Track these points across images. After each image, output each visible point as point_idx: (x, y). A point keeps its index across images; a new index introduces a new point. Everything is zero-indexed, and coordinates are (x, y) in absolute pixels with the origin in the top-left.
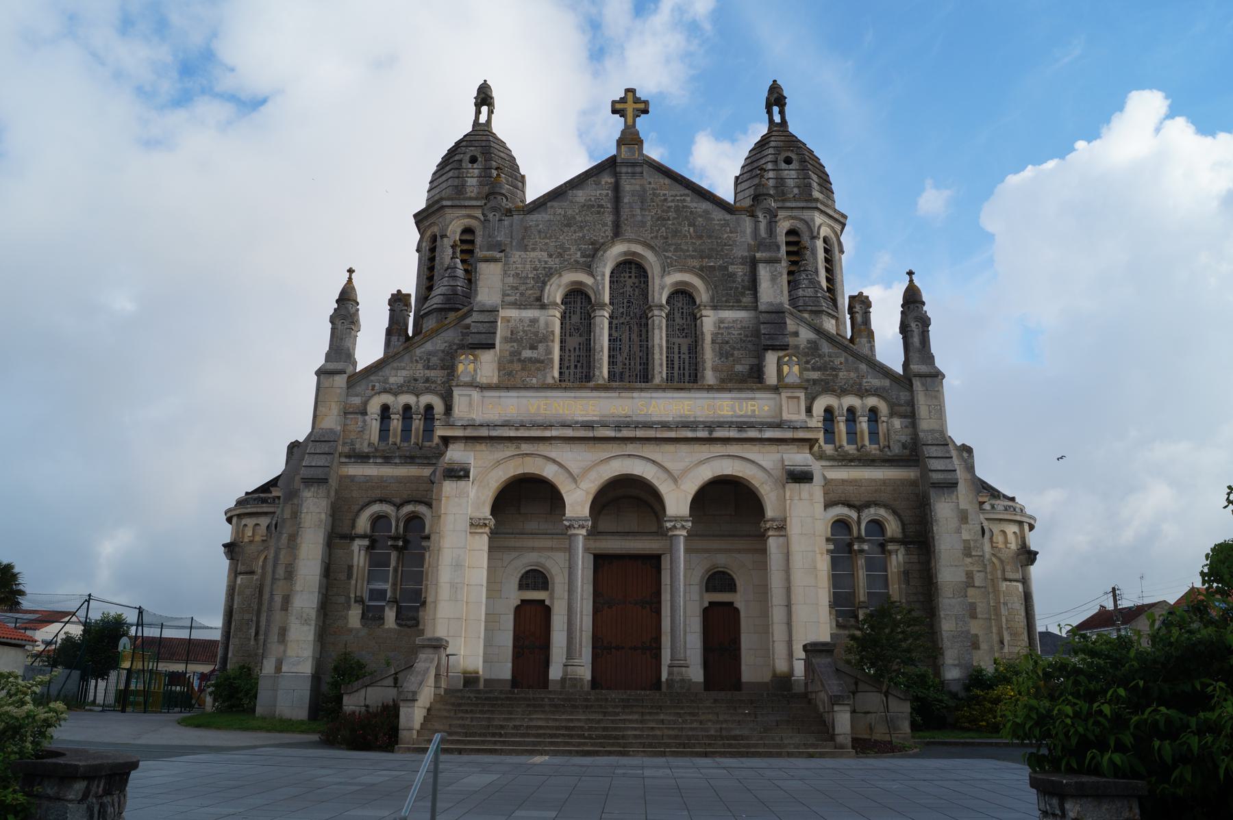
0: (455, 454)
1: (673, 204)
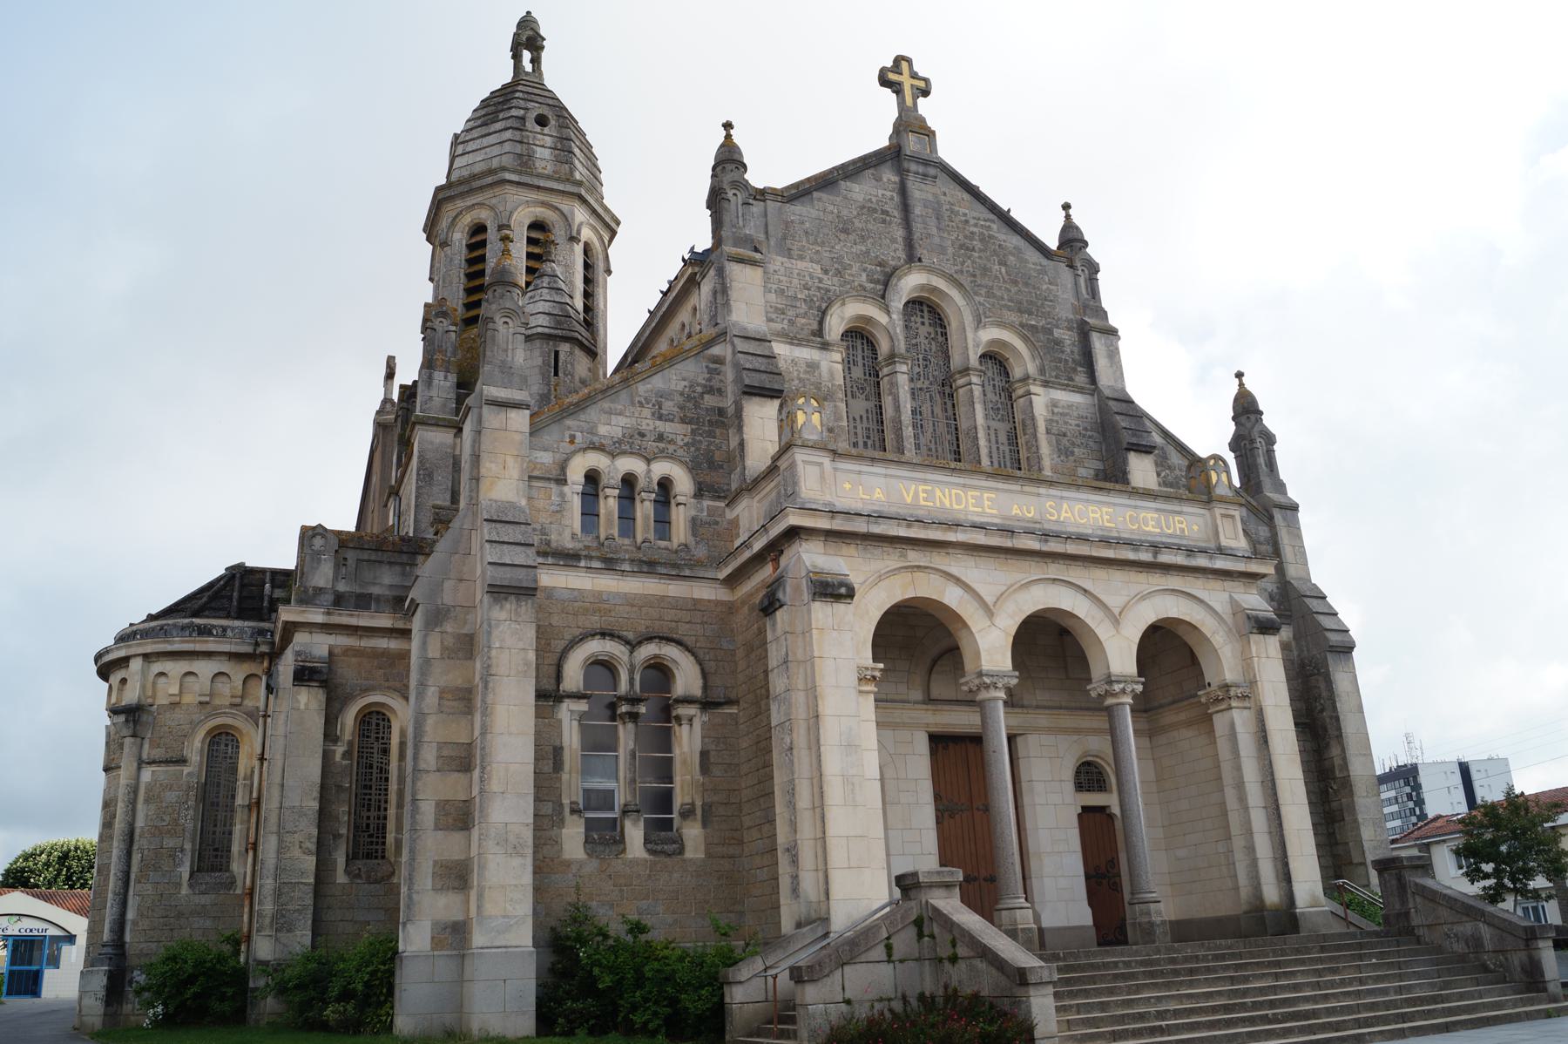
0: (811, 557)
1: (975, 230)
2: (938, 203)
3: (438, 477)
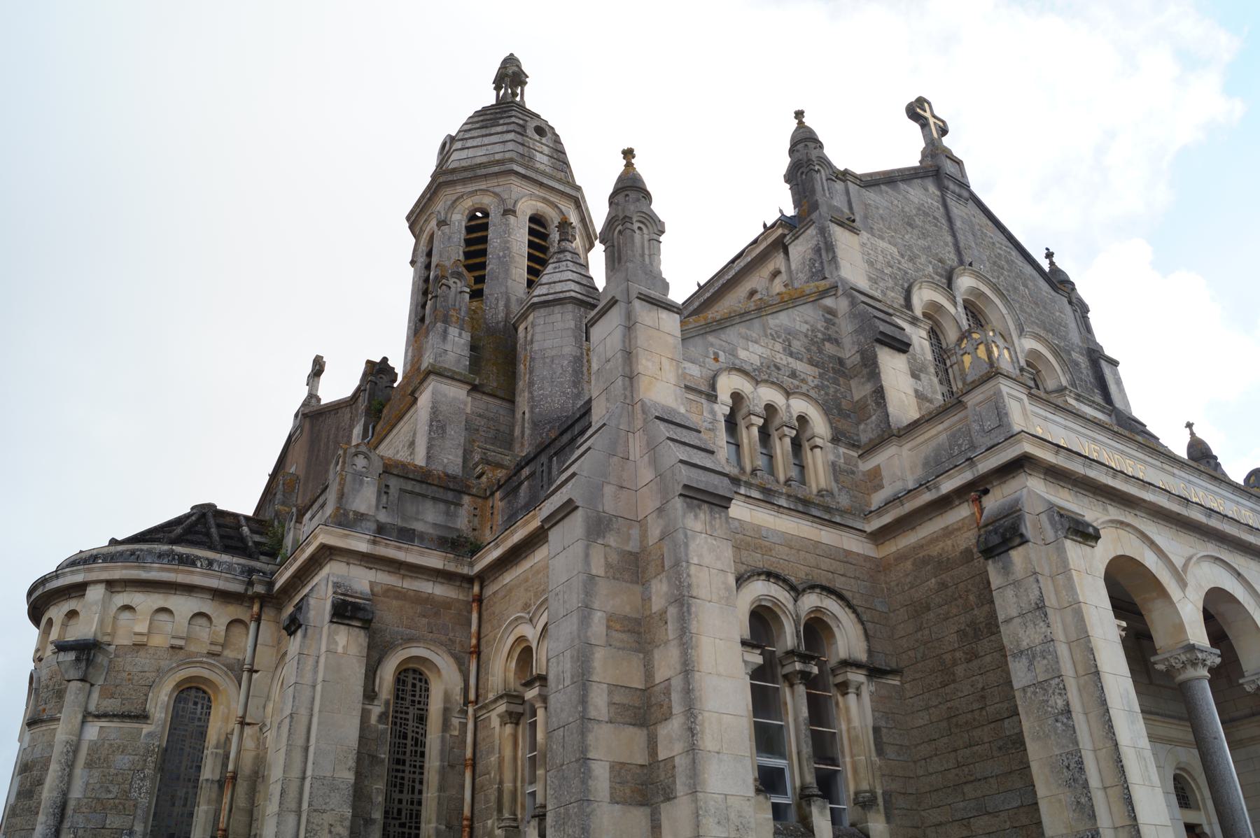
2: (971, 221)
3: (451, 431)
